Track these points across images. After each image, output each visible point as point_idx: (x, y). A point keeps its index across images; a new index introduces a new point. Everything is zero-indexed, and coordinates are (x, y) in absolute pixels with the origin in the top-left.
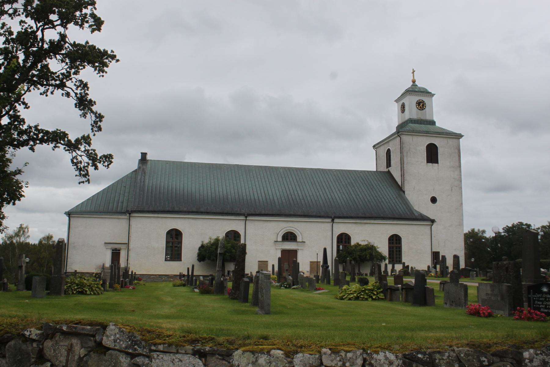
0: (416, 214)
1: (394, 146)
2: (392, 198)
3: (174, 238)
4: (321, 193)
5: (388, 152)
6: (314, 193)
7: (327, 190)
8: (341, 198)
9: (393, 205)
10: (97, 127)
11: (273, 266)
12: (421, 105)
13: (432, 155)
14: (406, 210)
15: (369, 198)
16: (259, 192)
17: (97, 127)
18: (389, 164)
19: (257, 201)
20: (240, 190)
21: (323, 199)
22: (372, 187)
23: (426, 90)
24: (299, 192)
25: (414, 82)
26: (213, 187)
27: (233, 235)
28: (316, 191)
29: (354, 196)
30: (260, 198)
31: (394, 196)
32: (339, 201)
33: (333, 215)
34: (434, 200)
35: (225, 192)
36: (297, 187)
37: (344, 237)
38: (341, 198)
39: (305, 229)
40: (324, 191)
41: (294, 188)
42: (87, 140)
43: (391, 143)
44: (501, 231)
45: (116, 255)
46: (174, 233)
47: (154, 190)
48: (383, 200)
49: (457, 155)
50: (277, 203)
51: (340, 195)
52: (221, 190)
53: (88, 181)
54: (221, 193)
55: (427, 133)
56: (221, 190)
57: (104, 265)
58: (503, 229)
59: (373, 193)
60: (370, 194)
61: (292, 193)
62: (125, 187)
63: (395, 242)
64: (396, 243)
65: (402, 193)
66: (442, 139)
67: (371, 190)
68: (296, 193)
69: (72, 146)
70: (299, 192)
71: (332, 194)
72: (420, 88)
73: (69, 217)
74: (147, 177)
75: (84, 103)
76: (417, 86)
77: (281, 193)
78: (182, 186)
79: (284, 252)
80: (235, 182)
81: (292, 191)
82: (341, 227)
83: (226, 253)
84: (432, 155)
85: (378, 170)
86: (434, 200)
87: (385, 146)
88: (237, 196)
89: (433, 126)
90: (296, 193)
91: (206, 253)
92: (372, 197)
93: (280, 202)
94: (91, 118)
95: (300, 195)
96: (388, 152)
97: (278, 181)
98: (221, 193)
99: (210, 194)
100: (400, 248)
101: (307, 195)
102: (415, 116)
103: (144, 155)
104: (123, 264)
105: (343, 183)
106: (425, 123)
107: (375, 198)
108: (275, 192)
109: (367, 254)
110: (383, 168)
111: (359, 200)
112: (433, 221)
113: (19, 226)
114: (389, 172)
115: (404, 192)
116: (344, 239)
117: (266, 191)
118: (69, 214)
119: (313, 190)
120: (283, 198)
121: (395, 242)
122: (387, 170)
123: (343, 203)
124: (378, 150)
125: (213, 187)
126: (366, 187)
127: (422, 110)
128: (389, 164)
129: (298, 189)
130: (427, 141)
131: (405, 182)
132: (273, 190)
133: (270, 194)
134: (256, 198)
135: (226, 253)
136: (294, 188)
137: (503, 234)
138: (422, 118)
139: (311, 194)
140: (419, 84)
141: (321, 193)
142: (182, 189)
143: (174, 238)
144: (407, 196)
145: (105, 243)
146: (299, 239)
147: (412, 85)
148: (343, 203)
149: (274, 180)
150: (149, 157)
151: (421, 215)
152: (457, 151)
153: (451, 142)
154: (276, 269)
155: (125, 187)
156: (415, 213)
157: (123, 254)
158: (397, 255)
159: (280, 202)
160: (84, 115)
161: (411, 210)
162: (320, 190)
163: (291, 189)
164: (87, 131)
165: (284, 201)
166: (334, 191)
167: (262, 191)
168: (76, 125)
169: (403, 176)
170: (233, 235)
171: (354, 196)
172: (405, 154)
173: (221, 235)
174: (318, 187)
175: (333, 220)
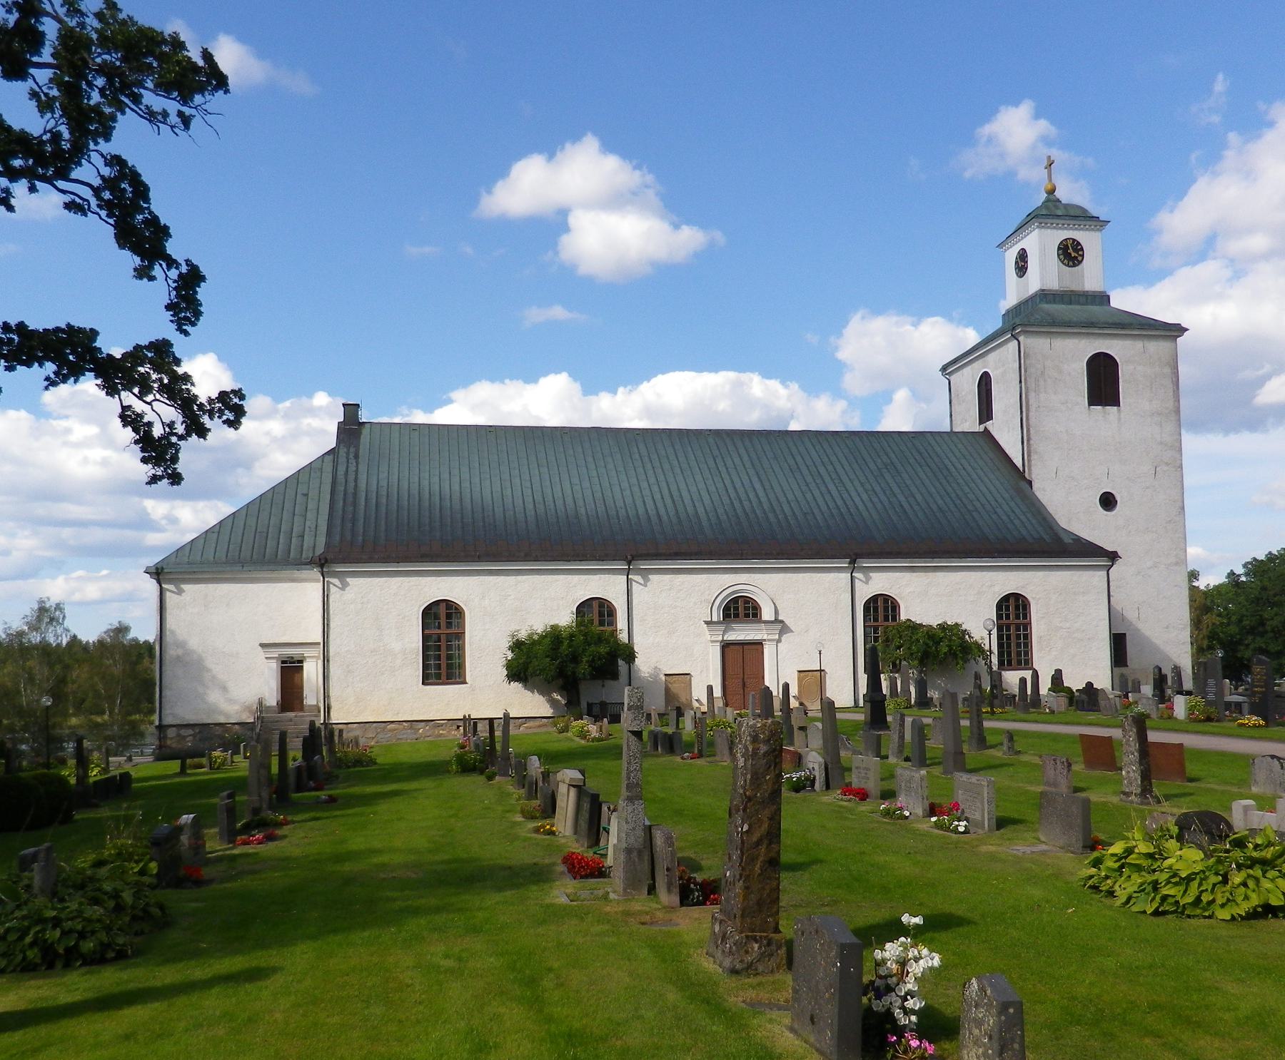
0: (1067, 540)
1: (1002, 363)
2: (1000, 500)
3: (442, 627)
4: (817, 493)
5: (985, 383)
6: (798, 494)
7: (831, 487)
8: (869, 505)
9: (1004, 518)
10: (185, 306)
11: (710, 689)
12: (1071, 254)
13: (1103, 383)
14: (1040, 529)
15: (940, 502)
16: (658, 496)
17: (185, 306)
18: (986, 412)
19: (654, 519)
20: (608, 493)
21: (824, 508)
22: (945, 472)
23: (1085, 211)
24: (761, 494)
25: (1051, 192)
26: (537, 486)
27: (596, 612)
28: (804, 488)
29: (902, 499)
30: (662, 512)
31: (1006, 496)
32: (865, 514)
33: (849, 545)
34: (1108, 501)
35: (569, 501)
36: (755, 479)
37: (880, 603)
38: (869, 505)
39: (772, 587)
40: (823, 489)
41: (746, 482)
42: (162, 353)
43: (992, 357)
44: (1240, 570)
45: (290, 671)
46: (442, 610)
47: (384, 500)
48: (978, 505)
49: (1168, 383)
50: (705, 523)
51: (865, 497)
52: (558, 494)
53: (176, 479)
54: (559, 503)
55: (1089, 327)
56: (558, 494)
57: (260, 703)
58: (1245, 566)
59: (950, 490)
60: (943, 492)
61: (743, 497)
62: (306, 495)
63: (1013, 611)
64: (1017, 617)
65: (1024, 485)
66: (1128, 343)
67: (944, 482)
68: (752, 495)
69: (116, 374)
70: (761, 494)
71: (845, 496)
72: (1067, 206)
73: (159, 582)
74: (363, 468)
75: (143, 238)
76: (1058, 201)
77: (716, 498)
78: (456, 487)
79: (726, 647)
80: (594, 474)
81: (741, 491)
82: (880, 581)
83: (579, 663)
84: (1103, 383)
85: (955, 430)
86: (1108, 501)
87: (976, 365)
88: (601, 509)
89: (1106, 308)
90: (752, 495)
91: (528, 662)
92: (948, 500)
93: (713, 520)
94: (161, 288)
95: (764, 500)
96: (985, 383)
97: (703, 466)
98: (559, 503)
99: (530, 506)
100: (1027, 626)
101: (783, 499)
102: (1053, 284)
103: (351, 410)
104: (311, 696)
105: (872, 466)
106: (1082, 300)
107: (958, 502)
108: (698, 495)
109: (942, 648)
110: (969, 422)
111: (916, 508)
112: (1113, 556)
113: (36, 607)
114: (987, 432)
115: (1030, 483)
116: (881, 610)
117: (675, 494)
118: (158, 573)
119: (795, 487)
120: (721, 511)
121: (1013, 611)
122: (982, 428)
123: (876, 516)
124: (953, 378)
125: (537, 486)
126: (930, 474)
127: (1074, 265)
128: (986, 412)
129: (758, 486)
130: (1085, 347)
131: (1034, 457)
132: (693, 489)
133: (688, 501)
134: (652, 512)
135: (579, 663)
136: (746, 482)
137: (1243, 579)
138: (1074, 288)
139: (790, 497)
140: (1063, 194)
141: (817, 493)
142: (456, 496)
143: (442, 627)
144: (1038, 494)
145: (262, 645)
146: (767, 614)
147: (1047, 200)
148: (876, 516)
149: (693, 463)
150: (364, 416)
151: (1078, 540)
152: (1167, 370)
153: (1157, 348)
154: (718, 692)
155: (306, 495)
156: (1063, 536)
157: (311, 671)
158: (1018, 645)
159: (713, 520)
160: (143, 273)
161: (1051, 528)
162: (813, 486)
163: (738, 485)
164: (161, 327)
165: (724, 517)
166: (849, 485)
167: (665, 492)
168: (126, 313)
169: (1025, 441)
170: (596, 612)
171: (902, 499)
172: (1032, 385)
173: (565, 618)
174: (809, 479)
175: (853, 562)
